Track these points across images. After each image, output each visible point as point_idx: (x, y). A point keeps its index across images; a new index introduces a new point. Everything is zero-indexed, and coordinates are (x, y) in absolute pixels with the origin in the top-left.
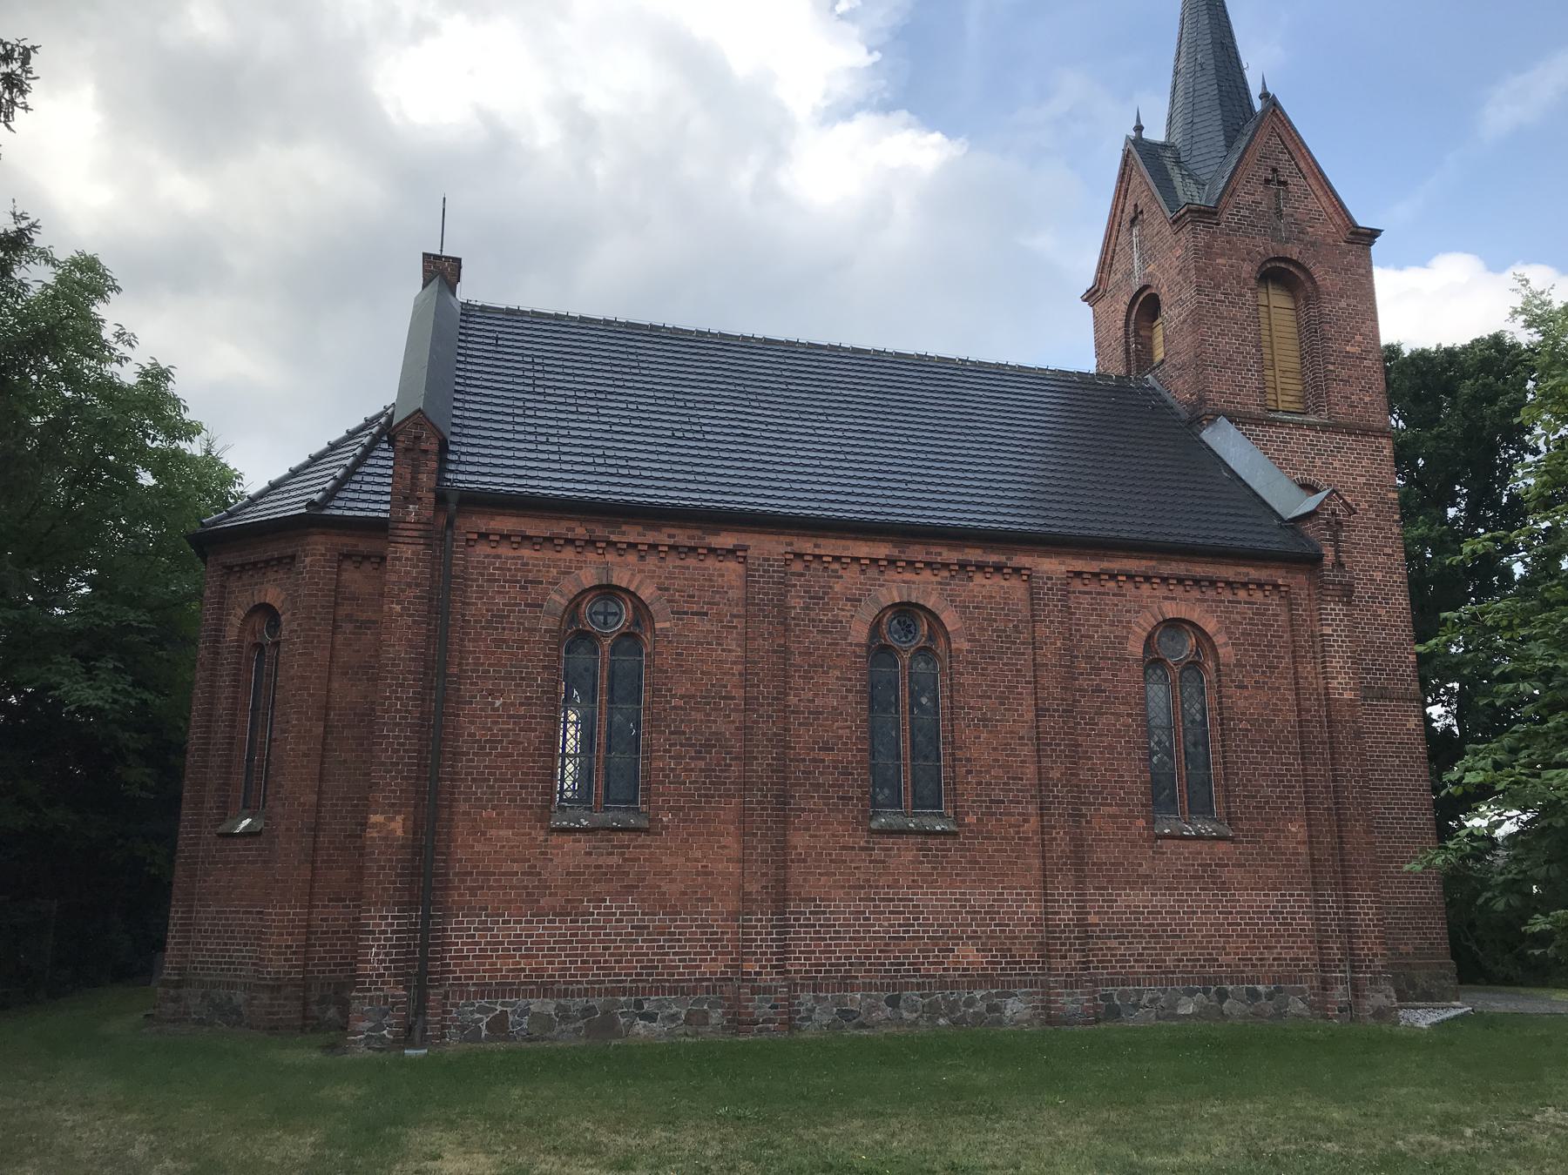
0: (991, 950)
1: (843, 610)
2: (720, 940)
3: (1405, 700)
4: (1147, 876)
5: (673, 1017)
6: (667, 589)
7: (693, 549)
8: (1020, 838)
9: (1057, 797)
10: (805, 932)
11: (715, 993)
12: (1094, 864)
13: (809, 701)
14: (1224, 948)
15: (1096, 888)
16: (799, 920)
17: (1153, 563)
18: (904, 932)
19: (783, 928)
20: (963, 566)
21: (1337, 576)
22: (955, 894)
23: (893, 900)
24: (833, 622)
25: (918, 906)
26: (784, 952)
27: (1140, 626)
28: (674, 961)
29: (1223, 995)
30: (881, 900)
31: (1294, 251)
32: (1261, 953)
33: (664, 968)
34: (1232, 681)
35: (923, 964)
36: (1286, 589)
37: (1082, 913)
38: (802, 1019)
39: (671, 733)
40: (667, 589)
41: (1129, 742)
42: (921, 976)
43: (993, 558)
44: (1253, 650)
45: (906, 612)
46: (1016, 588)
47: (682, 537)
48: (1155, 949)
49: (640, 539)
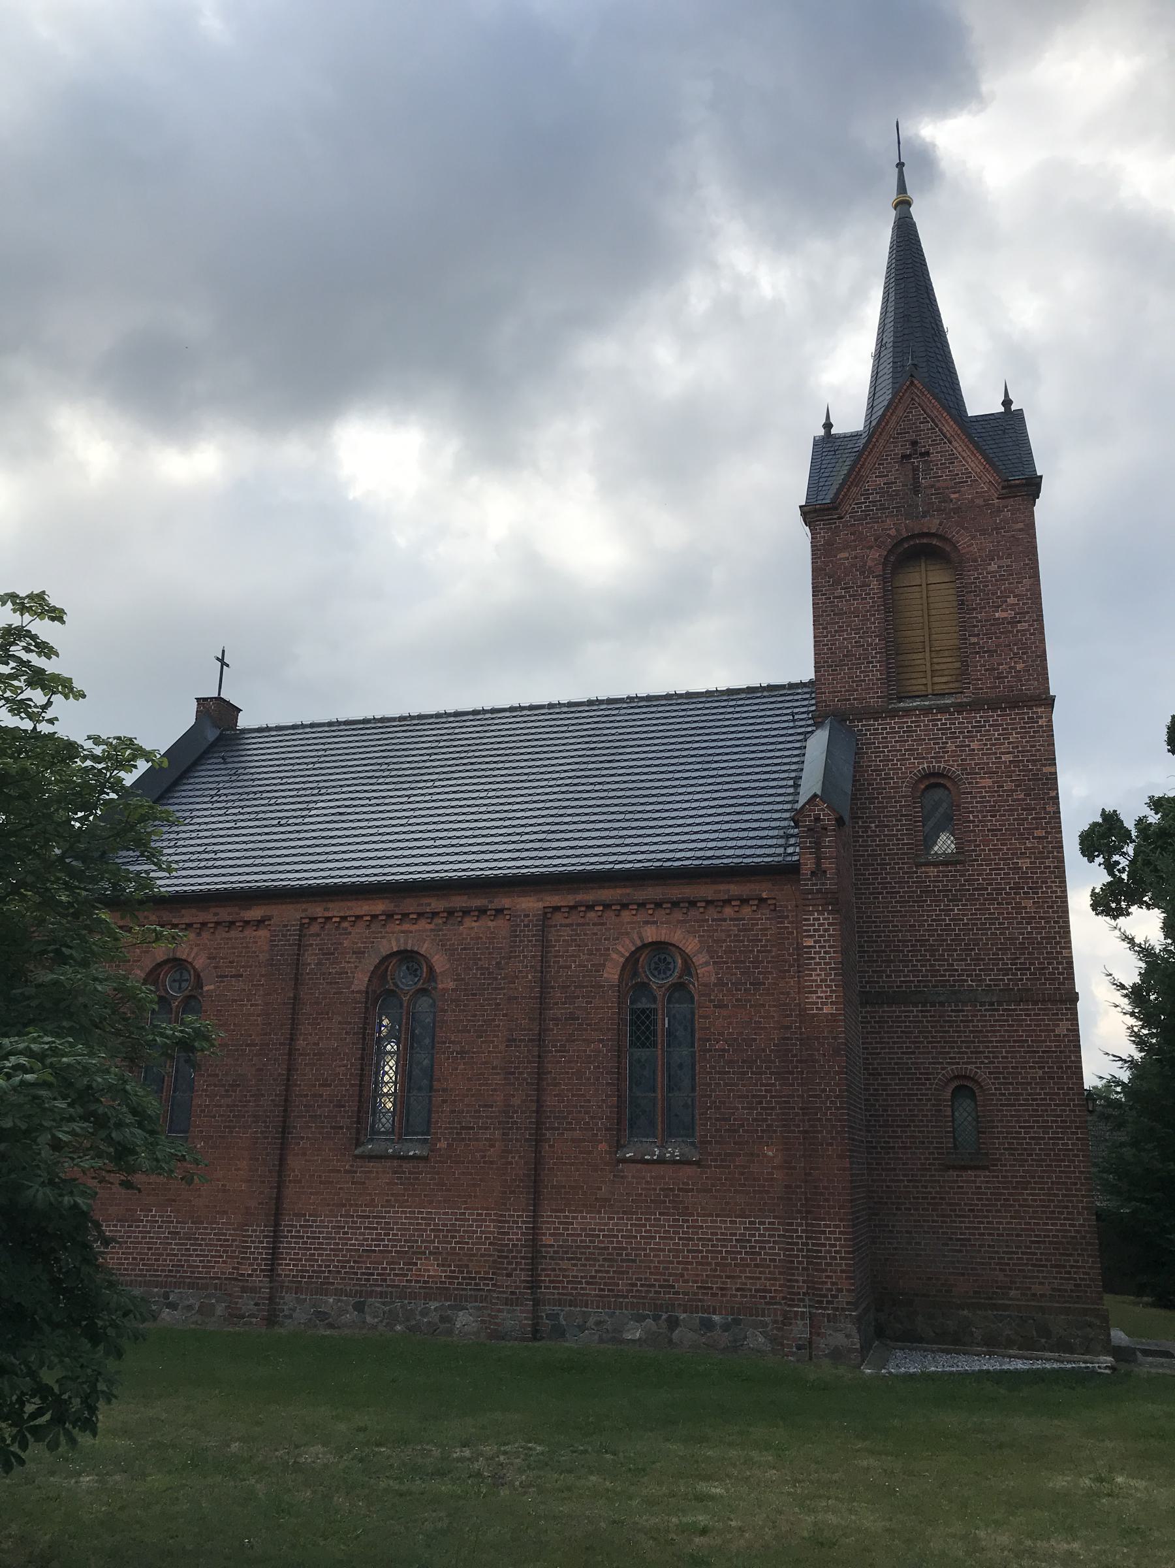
0: (450, 1266)
1: (349, 962)
2: (231, 1246)
3: (1054, 1002)
4: (607, 1200)
5: (189, 1307)
6: (214, 958)
7: (232, 923)
8: (485, 1162)
9: (516, 1123)
10: (295, 1243)
11: (221, 1290)
12: (553, 1187)
13: (315, 1044)
14: (682, 1275)
15: (553, 1211)
16: (291, 1231)
17: (628, 891)
18: (376, 1246)
19: (276, 1237)
20: (451, 913)
21: (816, 885)
22: (405, 1212)
23: (369, 1217)
24: (341, 973)
25: (389, 1223)
26: (274, 1255)
27: (619, 953)
28: (196, 1261)
29: (673, 1323)
30: (359, 1217)
31: (932, 524)
32: (723, 1283)
33: (189, 1266)
34: (711, 1001)
35: (389, 1275)
36: (774, 902)
37: (535, 1231)
38: (285, 1316)
39: (209, 1075)
40: (214, 958)
41: (598, 1067)
42: (388, 1286)
43: (477, 902)
44: (736, 968)
45: (408, 957)
46: (500, 926)
47: (225, 914)
48: (608, 1272)
49: (195, 920)
